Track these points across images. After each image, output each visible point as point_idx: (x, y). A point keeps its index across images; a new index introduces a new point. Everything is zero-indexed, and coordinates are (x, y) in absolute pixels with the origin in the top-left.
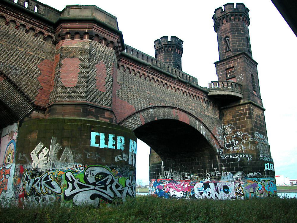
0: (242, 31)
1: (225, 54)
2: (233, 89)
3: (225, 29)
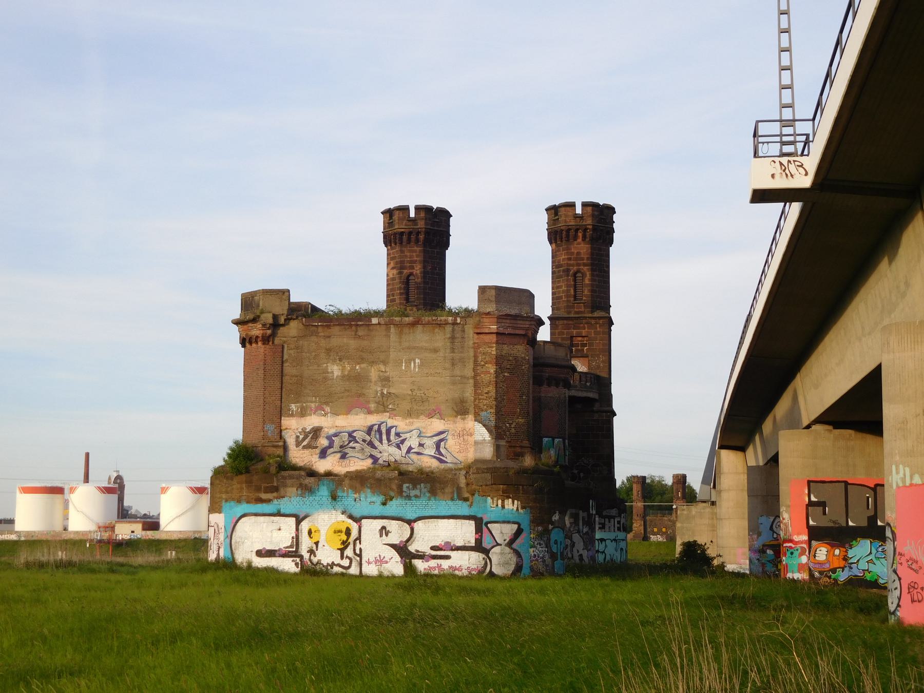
3: (578, 253)
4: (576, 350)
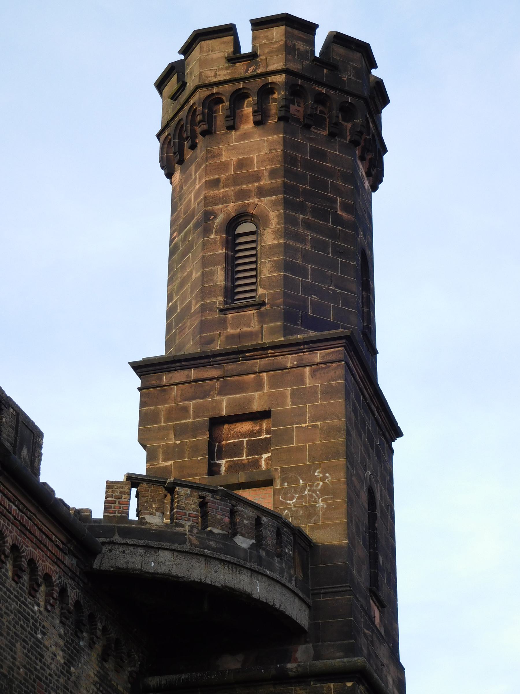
0: (346, 208)
1: (222, 324)
2: (260, 557)
3: (241, 164)
4: (232, 468)
